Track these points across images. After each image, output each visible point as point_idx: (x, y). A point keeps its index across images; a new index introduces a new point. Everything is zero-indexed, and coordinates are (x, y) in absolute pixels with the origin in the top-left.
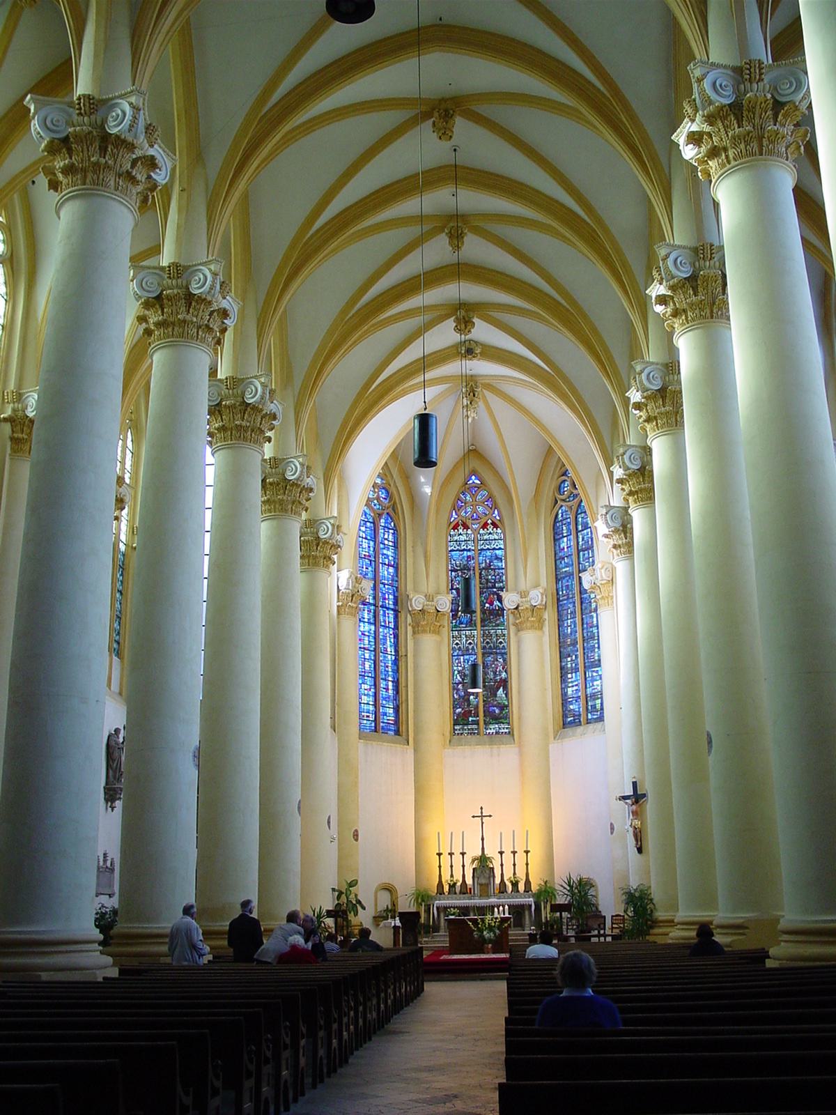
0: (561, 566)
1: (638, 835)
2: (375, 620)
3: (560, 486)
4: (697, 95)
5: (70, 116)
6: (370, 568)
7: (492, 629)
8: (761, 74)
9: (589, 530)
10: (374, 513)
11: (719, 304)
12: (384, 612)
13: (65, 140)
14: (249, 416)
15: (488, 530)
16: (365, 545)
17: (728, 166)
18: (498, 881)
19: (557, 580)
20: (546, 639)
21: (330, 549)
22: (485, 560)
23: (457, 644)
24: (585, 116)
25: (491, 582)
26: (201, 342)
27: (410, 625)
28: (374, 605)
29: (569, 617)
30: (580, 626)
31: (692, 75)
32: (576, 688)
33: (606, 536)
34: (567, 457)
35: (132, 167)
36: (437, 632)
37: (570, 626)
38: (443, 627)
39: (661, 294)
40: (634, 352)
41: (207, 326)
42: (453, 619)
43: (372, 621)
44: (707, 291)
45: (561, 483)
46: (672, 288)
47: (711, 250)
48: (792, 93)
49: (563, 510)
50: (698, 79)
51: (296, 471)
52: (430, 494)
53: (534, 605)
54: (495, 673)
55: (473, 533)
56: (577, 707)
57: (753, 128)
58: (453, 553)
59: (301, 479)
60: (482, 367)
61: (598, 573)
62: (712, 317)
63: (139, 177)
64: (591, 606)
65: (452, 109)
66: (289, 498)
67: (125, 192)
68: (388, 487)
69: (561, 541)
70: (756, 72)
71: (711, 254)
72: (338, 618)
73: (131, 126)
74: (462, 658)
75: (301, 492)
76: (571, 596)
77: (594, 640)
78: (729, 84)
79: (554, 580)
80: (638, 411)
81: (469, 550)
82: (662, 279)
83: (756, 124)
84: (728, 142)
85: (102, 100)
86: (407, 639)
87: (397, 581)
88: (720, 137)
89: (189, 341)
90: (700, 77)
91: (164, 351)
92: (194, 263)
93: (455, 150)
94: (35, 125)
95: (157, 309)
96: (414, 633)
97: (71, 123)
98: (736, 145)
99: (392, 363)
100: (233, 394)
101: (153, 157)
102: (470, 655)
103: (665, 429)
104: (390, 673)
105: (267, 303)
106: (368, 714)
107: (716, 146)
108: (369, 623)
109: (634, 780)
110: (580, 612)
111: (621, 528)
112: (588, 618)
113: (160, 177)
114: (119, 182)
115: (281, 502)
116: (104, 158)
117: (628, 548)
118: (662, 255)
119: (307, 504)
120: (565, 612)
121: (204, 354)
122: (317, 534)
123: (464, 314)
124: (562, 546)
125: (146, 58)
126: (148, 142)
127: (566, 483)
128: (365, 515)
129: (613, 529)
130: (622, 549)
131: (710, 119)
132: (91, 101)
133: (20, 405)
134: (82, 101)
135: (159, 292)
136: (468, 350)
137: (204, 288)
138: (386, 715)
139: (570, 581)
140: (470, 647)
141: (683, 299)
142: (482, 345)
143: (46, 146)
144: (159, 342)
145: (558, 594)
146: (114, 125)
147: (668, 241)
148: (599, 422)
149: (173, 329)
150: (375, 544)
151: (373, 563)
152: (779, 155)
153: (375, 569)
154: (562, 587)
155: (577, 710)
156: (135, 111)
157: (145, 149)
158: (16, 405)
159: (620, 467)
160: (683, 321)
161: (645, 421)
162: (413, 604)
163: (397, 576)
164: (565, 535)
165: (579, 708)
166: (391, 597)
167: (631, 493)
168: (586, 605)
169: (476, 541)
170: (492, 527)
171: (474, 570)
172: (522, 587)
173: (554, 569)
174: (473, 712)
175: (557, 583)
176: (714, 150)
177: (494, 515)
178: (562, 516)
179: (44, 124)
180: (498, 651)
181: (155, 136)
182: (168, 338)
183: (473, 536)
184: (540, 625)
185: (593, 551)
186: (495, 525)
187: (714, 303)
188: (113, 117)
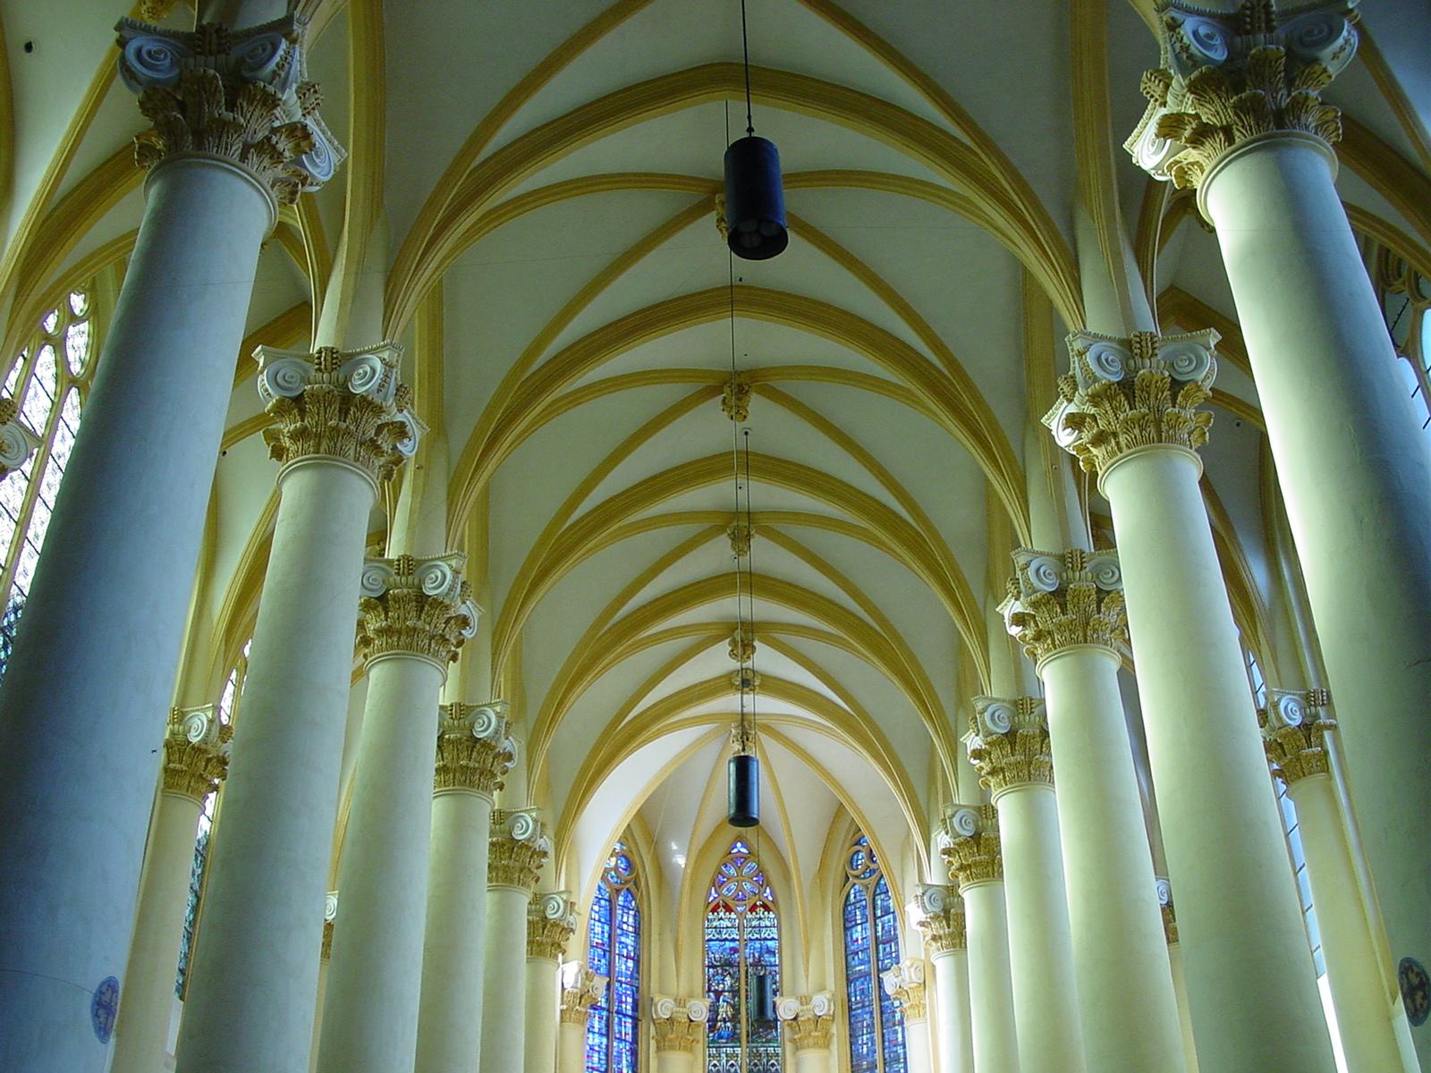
0: (853, 963)
2: (608, 1031)
3: (852, 858)
4: (1078, 370)
5: (306, 371)
6: (603, 961)
7: (762, 1047)
8: (1154, 349)
9: (891, 916)
10: (610, 887)
11: (1094, 625)
12: (620, 1020)
13: (298, 400)
14: (478, 753)
16: (598, 930)
17: (1120, 455)
19: (849, 981)
20: (834, 1060)
21: (560, 933)
23: (715, 1066)
24: (918, 398)
26: (433, 656)
27: (653, 1038)
28: (608, 1010)
29: (865, 1032)
30: (881, 1046)
31: (1069, 348)
33: (922, 924)
34: (863, 818)
35: (377, 434)
36: (689, 1048)
37: (867, 1044)
38: (698, 1042)
39: (1016, 612)
40: (966, 684)
41: (443, 636)
42: (710, 1031)
43: (604, 1031)
44: (1079, 608)
45: (855, 854)
46: (1034, 605)
47: (1082, 558)
48: (1192, 371)
49: (856, 890)
50: (1079, 352)
51: (527, 830)
52: (683, 866)
53: (819, 1014)
55: (738, 917)
57: (1149, 409)
58: (711, 943)
59: (533, 840)
60: (763, 704)
61: (905, 974)
62: (1086, 642)
63: (385, 447)
64: (894, 1017)
65: (747, 384)
66: (517, 864)
67: (367, 464)
68: (629, 855)
69: (854, 930)
70: (1147, 347)
71: (1082, 563)
72: (561, 1026)
73: (381, 386)
75: (531, 857)
76: (867, 1003)
77: (899, 1063)
78: (1117, 359)
79: (845, 983)
80: (978, 761)
81: (733, 940)
82: (1019, 593)
83: (1151, 405)
84: (1118, 426)
85: (348, 355)
86: (649, 1058)
87: (637, 979)
88: (1108, 421)
89: (417, 654)
90: (1082, 350)
91: (386, 666)
92: (430, 557)
93: (746, 433)
94: (263, 380)
95: (378, 612)
96: (658, 1049)
97: (306, 380)
98: (1127, 429)
99: (650, 694)
100: (459, 726)
101: (402, 424)
103: (1016, 784)
105: (506, 612)
107: (1103, 431)
108: (601, 1034)
110: (880, 1026)
111: (942, 914)
112: (891, 1034)
113: (408, 448)
114: (360, 452)
115: (506, 869)
116: (345, 421)
117: (956, 938)
118: (1020, 564)
119: (538, 872)
120: (859, 1024)
121: (437, 672)
122: (544, 913)
123: (744, 635)
124: (854, 937)
125: (404, 304)
126: (397, 406)
127: (861, 854)
128: (599, 891)
129: (932, 914)
130: (944, 942)
131: (1095, 399)
132: (334, 356)
133: (181, 727)
134: (323, 354)
135: (381, 593)
136: (746, 682)
137: (441, 589)
139: (866, 983)
141: (1048, 619)
142: (761, 675)
143: (274, 405)
144: (379, 655)
145: (849, 1000)
146: (359, 385)
147: (1023, 545)
148: (909, 770)
149: (399, 638)
150: (610, 929)
151: (607, 954)
153: (610, 963)
154: (855, 991)
156: (387, 368)
157: (393, 414)
158: (176, 726)
159: (947, 833)
160: (1048, 645)
161: (988, 774)
162: (659, 1010)
163: (638, 973)
164: (859, 922)
166: (630, 1000)
167: (962, 868)
168: (888, 1016)
169: (741, 928)
170: (724, 910)
171: (739, 966)
172: (803, 989)
173: (844, 967)
175: (848, 986)
176: (1101, 435)
177: (765, 895)
178: (855, 897)
179: (274, 380)
181: (406, 399)
182: (392, 649)
183: (737, 921)
185: (897, 944)
186: (766, 908)
187: (1088, 624)
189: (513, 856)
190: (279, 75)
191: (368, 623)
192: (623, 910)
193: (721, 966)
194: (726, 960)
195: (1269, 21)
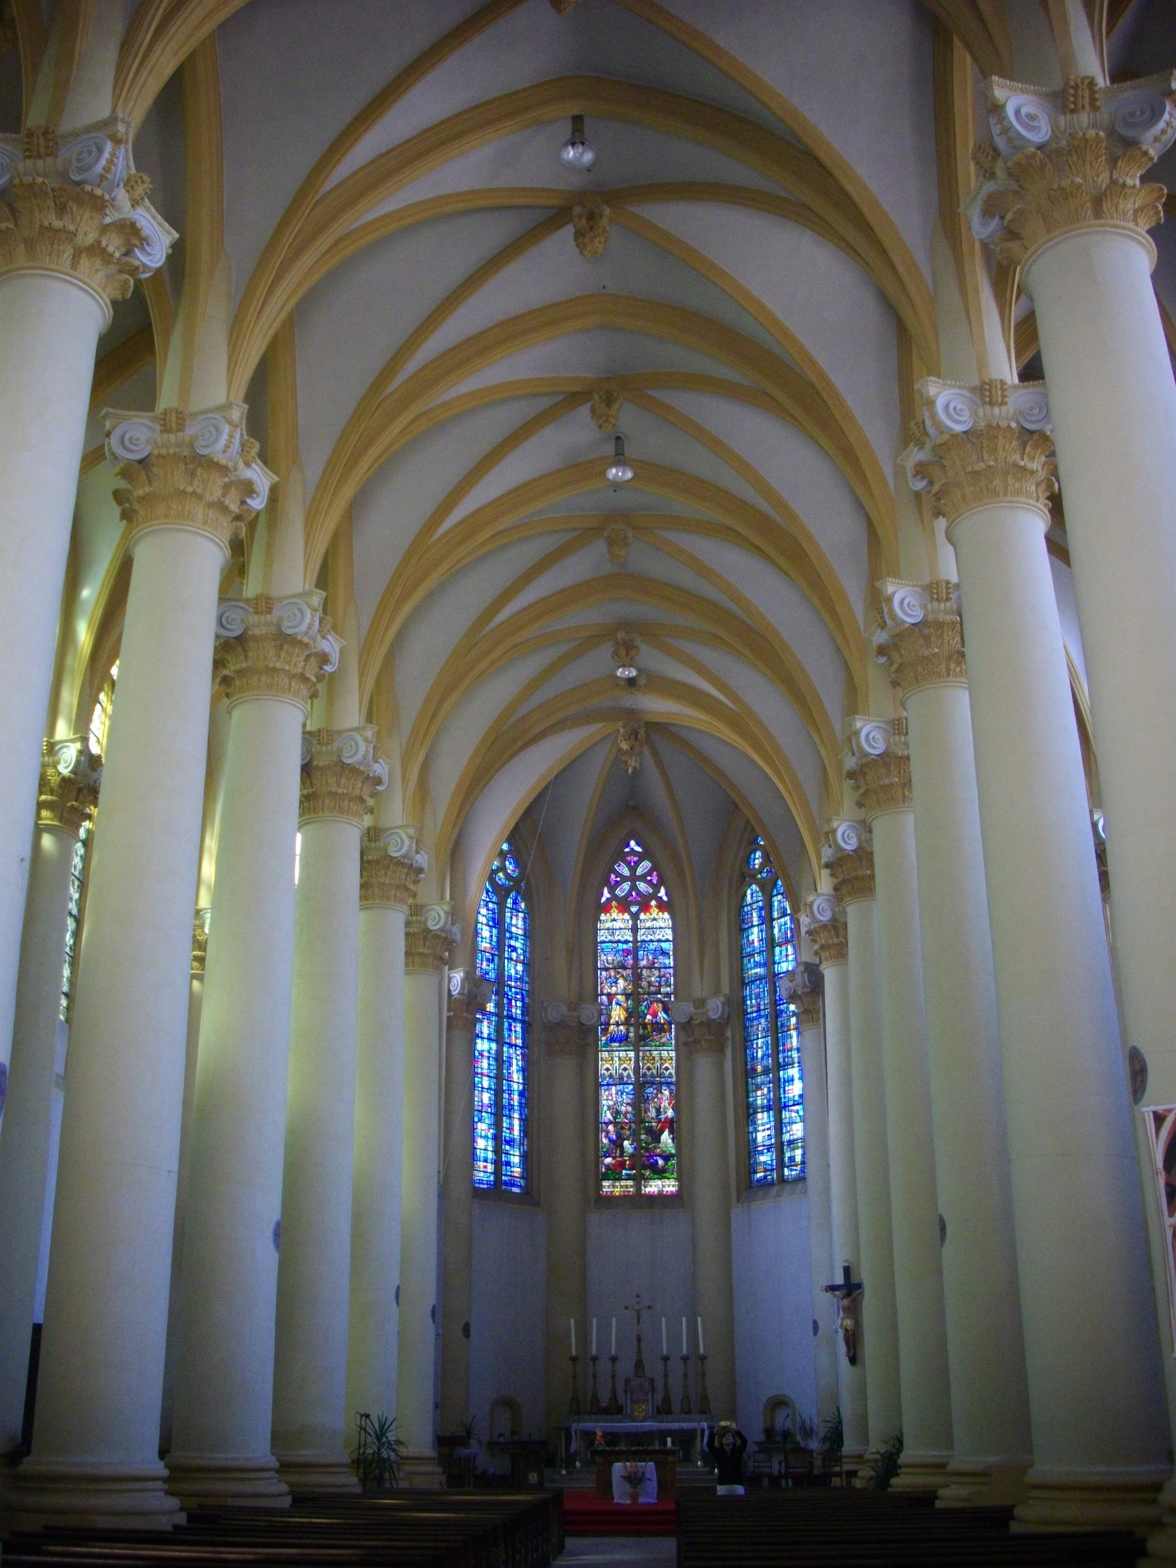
1: (853, 1340)
8: (1004, 396)
12: (510, 1025)
54: (658, 1111)
56: (769, 1159)
74: (614, 1088)
102: (624, 1084)
104: (516, 1108)
106: (485, 1164)
108: (489, 1039)
109: (846, 1264)
138: (510, 1166)
139: (761, 986)
151: (496, 958)
152: (1028, 495)
155: (769, 1162)
165: (772, 1160)
174: (627, 1163)
178: (752, 897)
180: (662, 1080)
184: (719, 1048)
188: (393, 844)
189: (389, 873)
190: (107, 179)
191: (228, 662)
192: (511, 912)
193: (614, 968)
194: (619, 962)
195: (1093, 100)
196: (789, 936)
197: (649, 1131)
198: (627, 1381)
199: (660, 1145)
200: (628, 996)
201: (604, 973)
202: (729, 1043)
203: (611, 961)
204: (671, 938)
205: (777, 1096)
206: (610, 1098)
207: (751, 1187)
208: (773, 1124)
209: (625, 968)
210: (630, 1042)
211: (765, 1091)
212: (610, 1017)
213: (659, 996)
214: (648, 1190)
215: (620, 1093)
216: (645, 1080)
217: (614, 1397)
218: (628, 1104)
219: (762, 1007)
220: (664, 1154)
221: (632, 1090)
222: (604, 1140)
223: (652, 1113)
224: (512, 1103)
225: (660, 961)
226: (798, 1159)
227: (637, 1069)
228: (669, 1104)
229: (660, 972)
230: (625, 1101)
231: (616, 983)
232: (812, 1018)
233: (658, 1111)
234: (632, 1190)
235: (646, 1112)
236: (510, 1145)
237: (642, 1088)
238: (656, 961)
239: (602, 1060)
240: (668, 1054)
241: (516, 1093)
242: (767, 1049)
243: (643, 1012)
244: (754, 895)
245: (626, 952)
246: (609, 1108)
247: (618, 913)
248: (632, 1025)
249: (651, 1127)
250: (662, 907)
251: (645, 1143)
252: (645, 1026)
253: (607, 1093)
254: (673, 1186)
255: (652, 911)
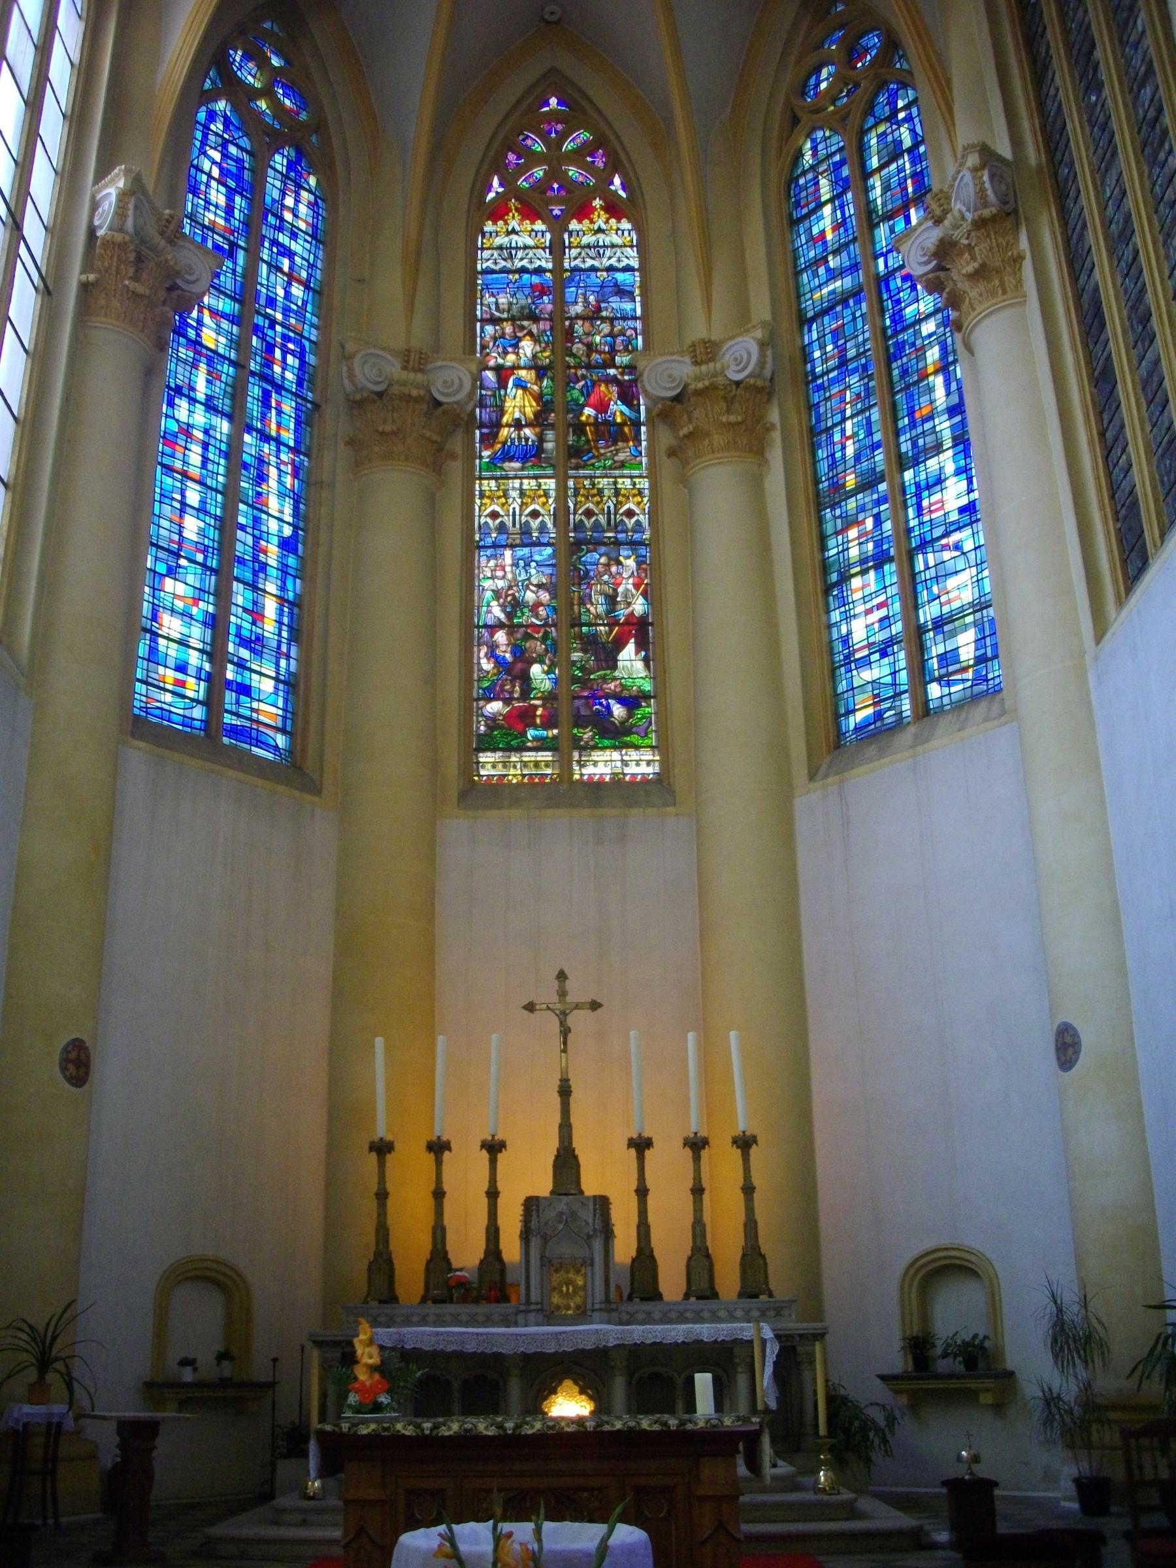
12: (266, 395)
15: (592, 222)
18: (624, 1248)
22: (584, 295)
25: (600, 353)
32: (883, 612)
54: (611, 600)
56: (887, 670)
74: (508, 553)
106: (180, 676)
108: (210, 405)
140: (535, 524)
174: (539, 712)
180: (621, 536)
194: (522, 308)
196: (910, 190)
197: (590, 643)
198: (531, 1205)
199: (617, 674)
200: (541, 371)
201: (489, 329)
202: (776, 436)
203: (506, 307)
204: (635, 264)
205: (902, 525)
206: (500, 573)
207: (838, 746)
208: (893, 590)
209: (535, 319)
210: (547, 459)
211: (869, 523)
212: (501, 411)
213: (612, 372)
214: (589, 770)
215: (521, 563)
216: (581, 535)
217: (493, 1251)
218: (540, 586)
219: (851, 353)
220: (625, 693)
221: (551, 557)
222: (484, 661)
223: (598, 606)
224: (262, 557)
225: (614, 305)
226: (967, 654)
227: (561, 514)
228: (637, 586)
229: (613, 326)
230: (534, 581)
231: (516, 346)
232: (1002, 285)
233: (611, 600)
234: (549, 771)
235: (582, 602)
236: (252, 650)
237: (573, 554)
238: (603, 305)
239: (482, 496)
240: (634, 484)
241: (275, 540)
242: (870, 434)
243: (576, 401)
244: (820, 147)
245: (542, 290)
246: (497, 594)
247: (522, 221)
248: (552, 426)
249: (596, 635)
250: (614, 209)
251: (582, 669)
252: (579, 428)
253: (492, 563)
254: (649, 763)
255: (595, 217)
